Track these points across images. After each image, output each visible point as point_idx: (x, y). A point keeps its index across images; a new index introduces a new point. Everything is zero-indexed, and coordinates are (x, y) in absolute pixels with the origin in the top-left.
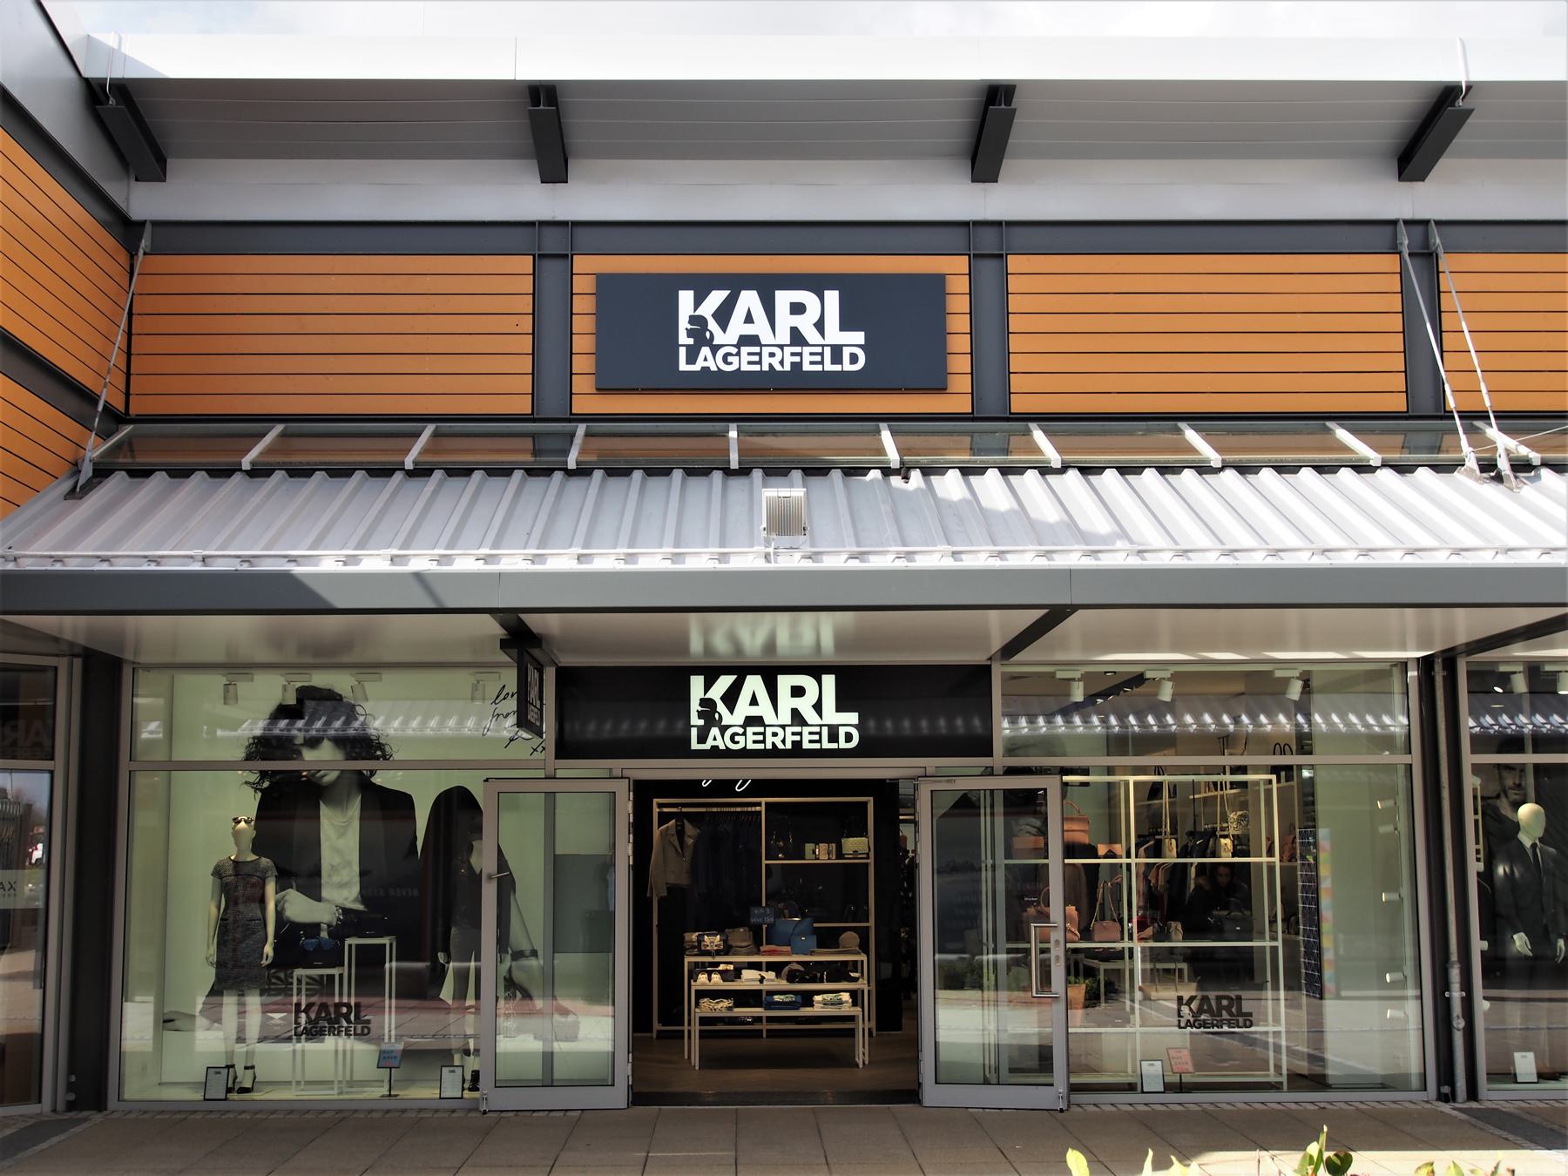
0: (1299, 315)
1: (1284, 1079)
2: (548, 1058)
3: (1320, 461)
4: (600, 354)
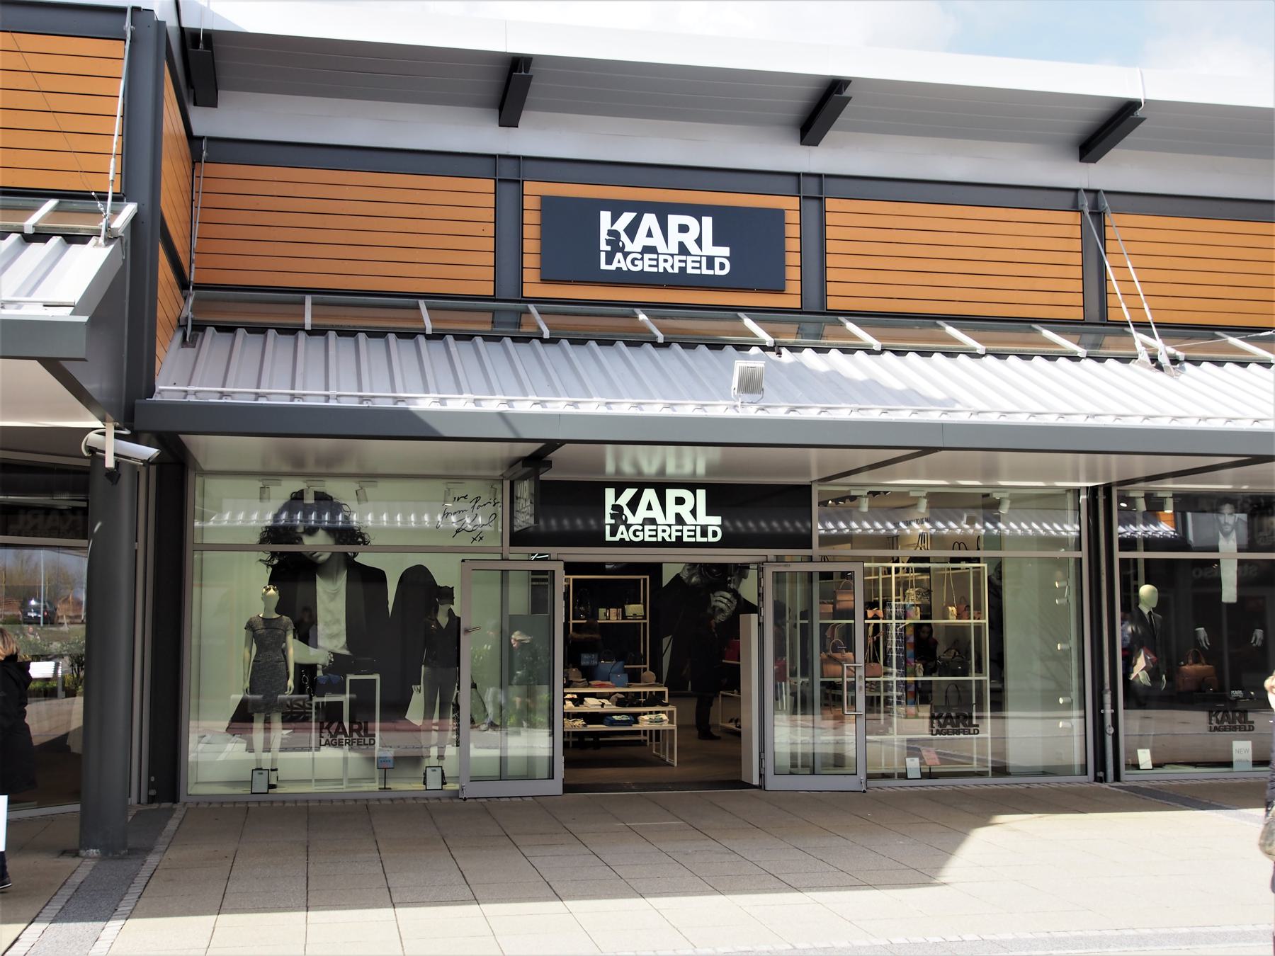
0: (1016, 250)
1: (990, 770)
2: (503, 760)
3: (844, 345)
4: (543, 254)
